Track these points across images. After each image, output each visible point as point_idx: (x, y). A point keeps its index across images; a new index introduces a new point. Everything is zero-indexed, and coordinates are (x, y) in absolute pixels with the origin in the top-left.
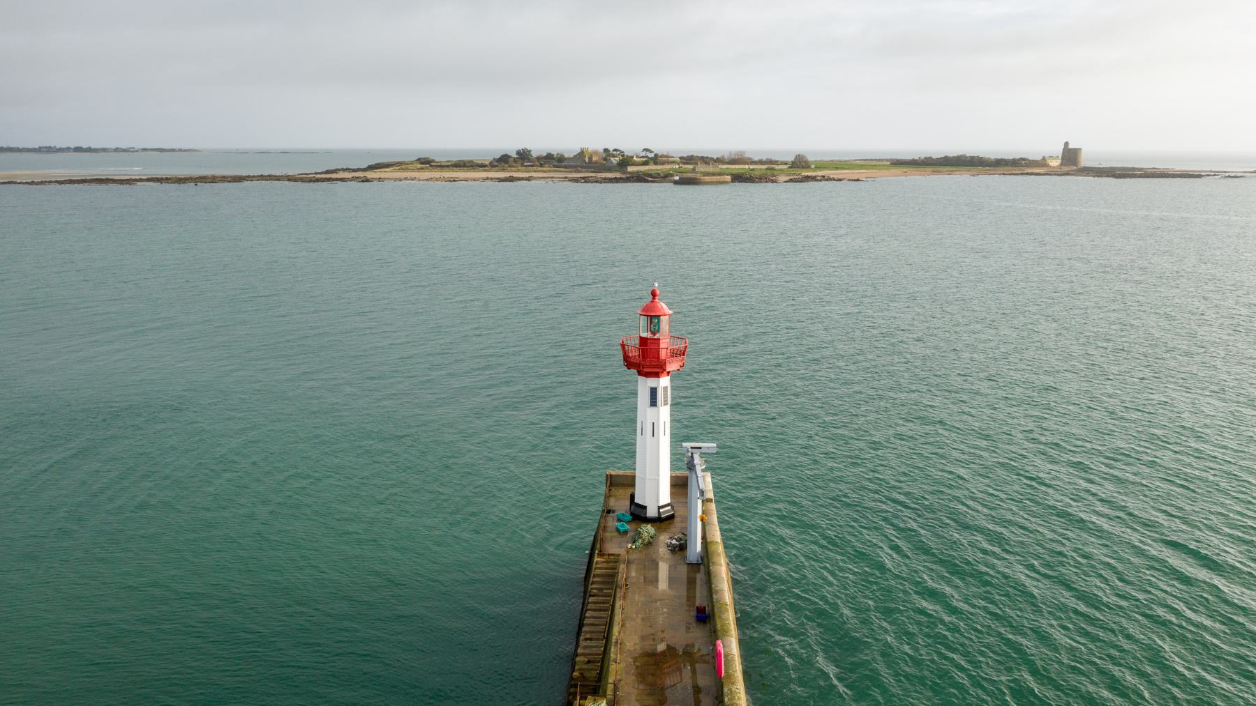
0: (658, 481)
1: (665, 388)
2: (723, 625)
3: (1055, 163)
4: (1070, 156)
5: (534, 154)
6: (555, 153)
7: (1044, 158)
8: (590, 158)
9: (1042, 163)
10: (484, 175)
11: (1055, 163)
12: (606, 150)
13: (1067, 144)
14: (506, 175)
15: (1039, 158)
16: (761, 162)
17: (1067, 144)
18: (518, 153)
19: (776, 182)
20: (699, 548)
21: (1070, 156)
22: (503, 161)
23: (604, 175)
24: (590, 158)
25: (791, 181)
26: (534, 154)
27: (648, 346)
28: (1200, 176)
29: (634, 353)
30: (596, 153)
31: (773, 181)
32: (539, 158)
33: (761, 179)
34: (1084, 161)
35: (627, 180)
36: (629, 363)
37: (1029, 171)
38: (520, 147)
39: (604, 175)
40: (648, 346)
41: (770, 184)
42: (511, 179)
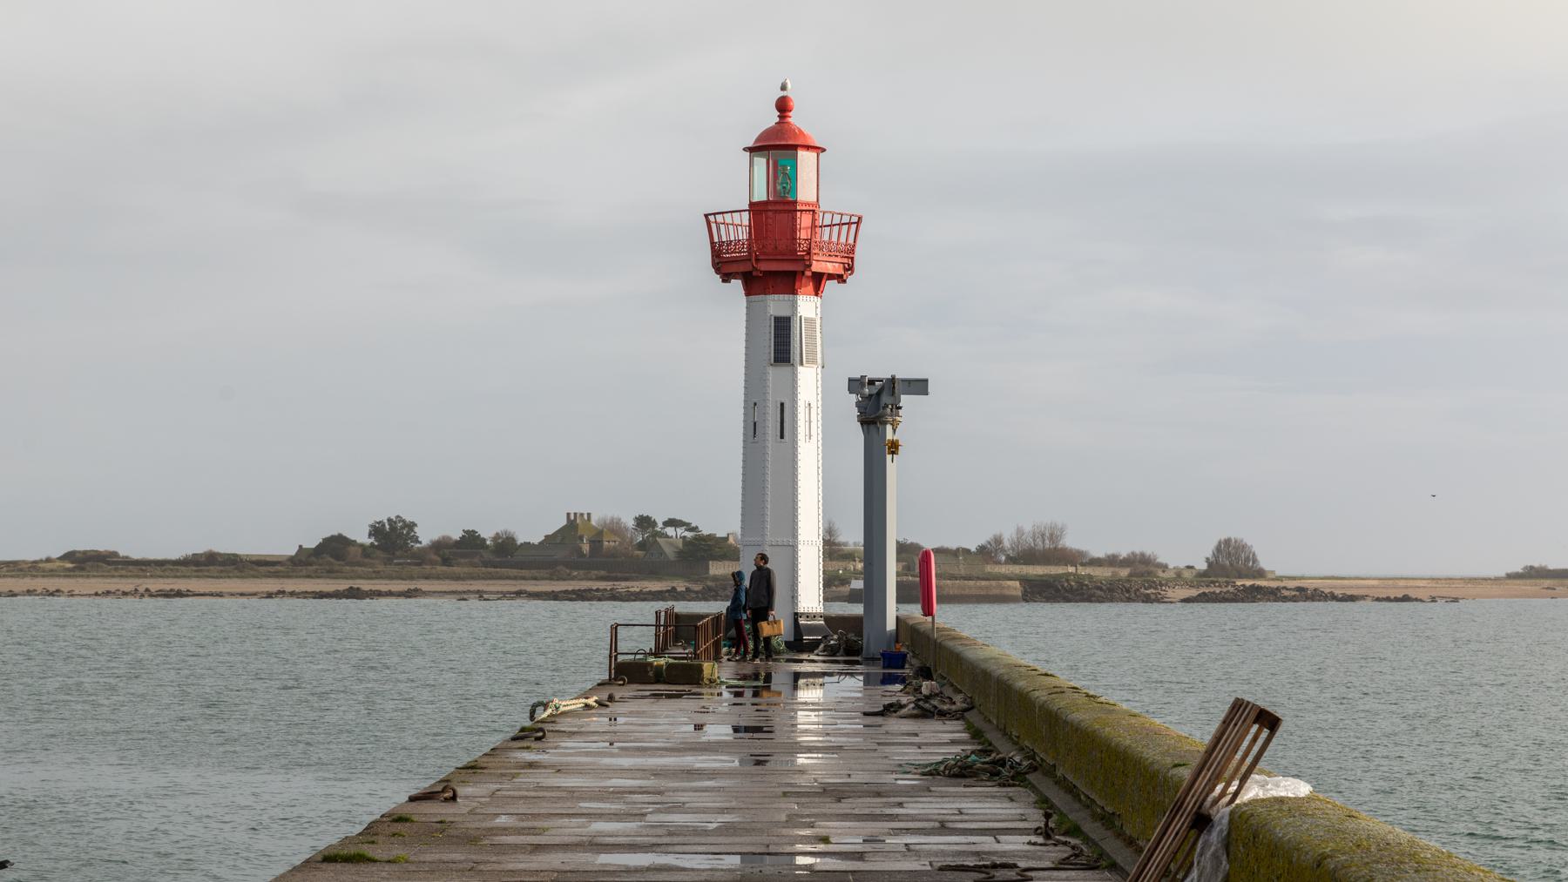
2: (1009, 666)
5: (426, 535)
8: (596, 542)
12: (644, 522)
13: (919, 386)
14: (343, 585)
16: (1112, 561)
17: (919, 386)
18: (376, 531)
19: (1159, 600)
22: (330, 558)
24: (596, 542)
25: (1203, 598)
26: (426, 535)
27: (775, 214)
28: (1352, 598)
29: (738, 230)
30: (615, 528)
31: (1147, 599)
35: (1234, 599)
36: (725, 264)
37: (635, 586)
38: (383, 514)
39: (635, 586)
40: (775, 214)
41: (1141, 607)
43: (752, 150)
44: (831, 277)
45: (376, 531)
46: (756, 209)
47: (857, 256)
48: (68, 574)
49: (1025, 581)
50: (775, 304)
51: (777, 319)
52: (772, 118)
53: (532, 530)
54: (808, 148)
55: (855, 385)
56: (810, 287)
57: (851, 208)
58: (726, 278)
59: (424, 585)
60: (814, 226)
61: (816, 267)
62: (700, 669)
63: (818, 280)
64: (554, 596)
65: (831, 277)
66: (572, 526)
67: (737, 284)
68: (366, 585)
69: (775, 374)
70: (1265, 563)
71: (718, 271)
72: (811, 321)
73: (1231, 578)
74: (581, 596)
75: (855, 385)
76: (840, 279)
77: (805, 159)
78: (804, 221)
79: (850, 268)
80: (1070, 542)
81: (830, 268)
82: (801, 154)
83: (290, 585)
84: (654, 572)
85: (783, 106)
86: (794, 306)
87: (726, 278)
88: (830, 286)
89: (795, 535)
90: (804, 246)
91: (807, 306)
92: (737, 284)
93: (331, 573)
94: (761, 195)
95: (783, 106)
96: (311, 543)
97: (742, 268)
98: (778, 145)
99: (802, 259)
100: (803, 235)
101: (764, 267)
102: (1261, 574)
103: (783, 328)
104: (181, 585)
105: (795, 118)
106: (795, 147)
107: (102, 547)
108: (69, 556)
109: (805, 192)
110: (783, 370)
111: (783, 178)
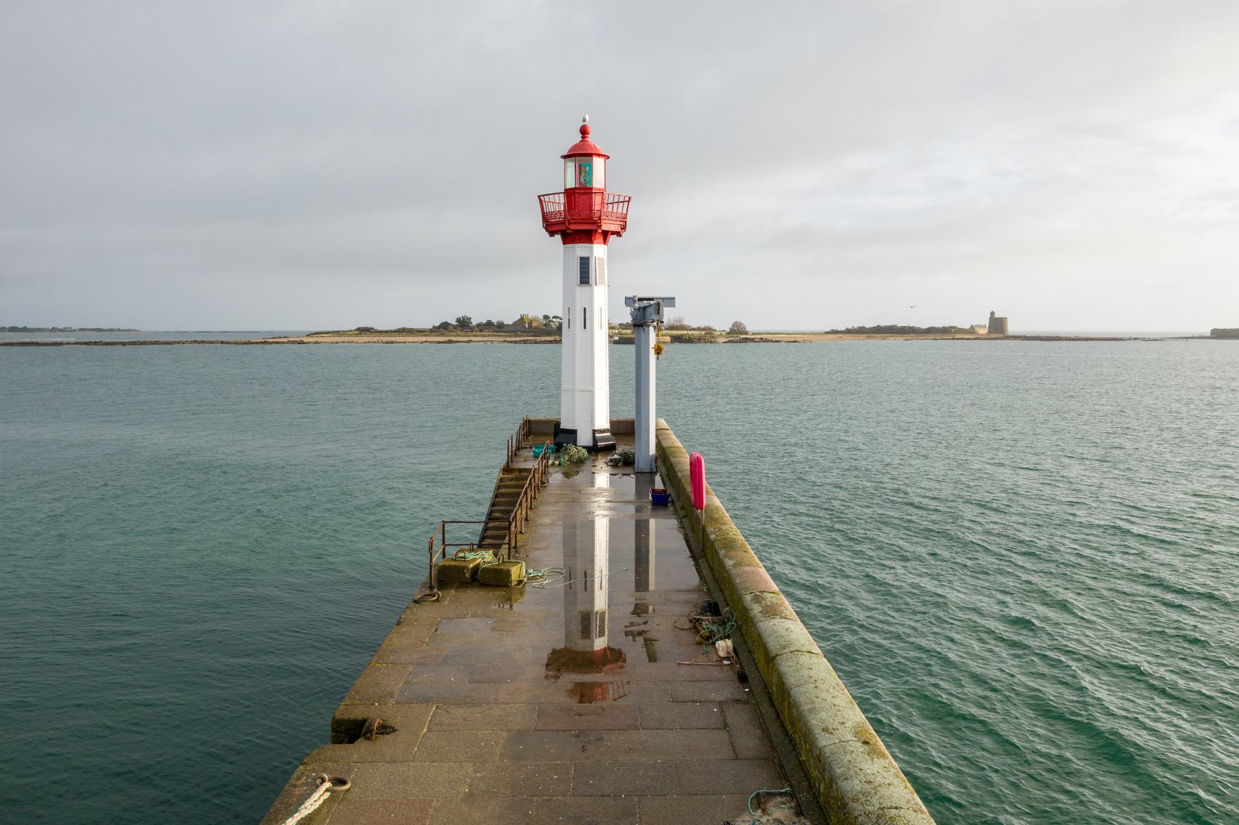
0: (592, 392)
1: (601, 634)
3: (983, 332)
4: (997, 326)
5: (474, 322)
6: (495, 321)
7: (972, 327)
8: (530, 324)
9: (972, 330)
10: (424, 339)
11: (983, 332)
12: (546, 317)
13: (992, 313)
14: (446, 339)
15: (967, 327)
16: (699, 329)
17: (992, 313)
18: (458, 320)
19: (696, 465)
20: (652, 450)
21: (997, 326)
23: (543, 339)
24: (530, 324)
25: (730, 342)
26: (474, 322)
27: (579, 196)
29: (558, 204)
30: (536, 320)
32: (479, 325)
33: (699, 340)
34: (1012, 328)
36: (551, 226)
39: (543, 339)
40: (579, 196)
42: (450, 342)
43: (565, 157)
44: (613, 233)
45: (458, 320)
46: (569, 193)
47: (628, 221)
48: (356, 335)
49: (671, 336)
50: (580, 249)
51: (581, 258)
52: (579, 137)
53: (509, 321)
54: (599, 155)
55: (629, 301)
56: (601, 239)
57: (625, 193)
58: (552, 234)
59: (474, 339)
60: (603, 203)
61: (604, 227)
62: (508, 574)
63: (606, 235)
64: (516, 342)
65: (613, 233)
66: (522, 320)
67: (558, 237)
68: (454, 339)
69: (581, 291)
70: (748, 329)
71: (546, 229)
72: (601, 260)
73: (738, 335)
74: (525, 342)
75: (629, 301)
76: (618, 234)
77: (598, 163)
78: (597, 200)
79: (624, 228)
80: (686, 323)
81: (613, 228)
82: (595, 159)
83: (429, 339)
84: (549, 334)
85: (584, 131)
86: (592, 251)
87: (552, 234)
88: (612, 238)
89: (593, 385)
90: (597, 215)
91: (598, 251)
92: (558, 237)
93: (443, 335)
94: (571, 184)
95: (584, 131)
96: (437, 324)
97: (560, 228)
98: (581, 155)
99: (595, 223)
100: (597, 207)
101: (573, 227)
102: (747, 333)
103: (585, 263)
104: (393, 339)
105: (591, 139)
106: (591, 155)
107: (369, 326)
108: (358, 329)
109: (598, 182)
110: (585, 288)
111: (584, 171)
